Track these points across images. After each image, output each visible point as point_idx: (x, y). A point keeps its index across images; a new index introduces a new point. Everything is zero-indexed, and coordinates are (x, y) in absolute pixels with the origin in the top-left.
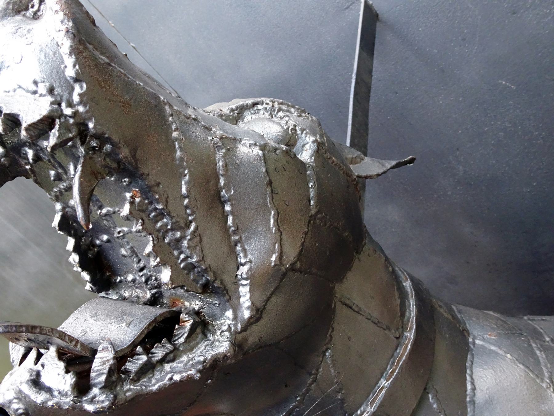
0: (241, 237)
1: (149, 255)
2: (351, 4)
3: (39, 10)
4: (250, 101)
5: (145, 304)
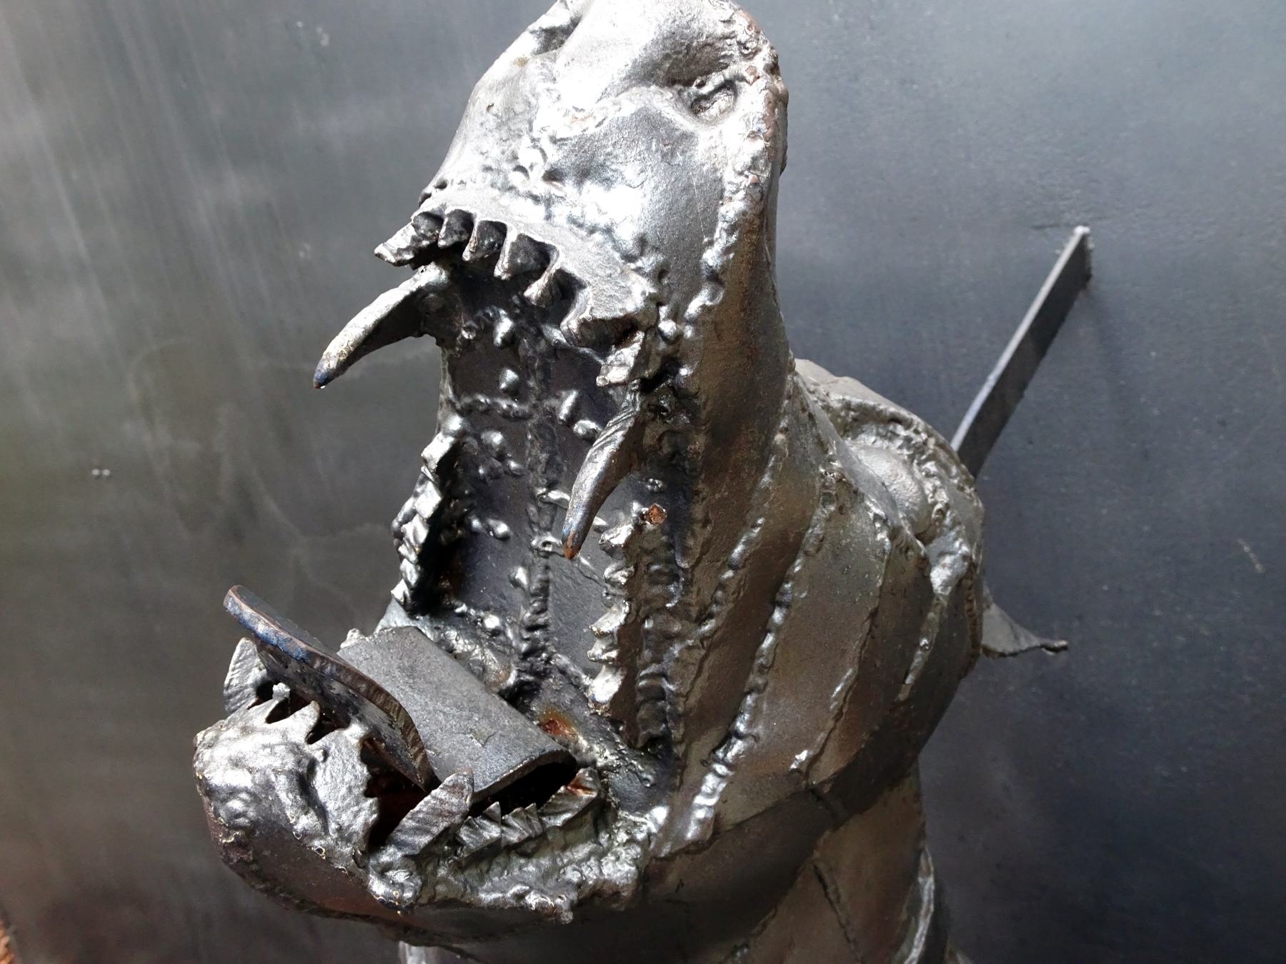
0: (766, 685)
1: (602, 635)
2: (1051, 226)
3: (707, 97)
4: (892, 409)
5: (502, 694)
